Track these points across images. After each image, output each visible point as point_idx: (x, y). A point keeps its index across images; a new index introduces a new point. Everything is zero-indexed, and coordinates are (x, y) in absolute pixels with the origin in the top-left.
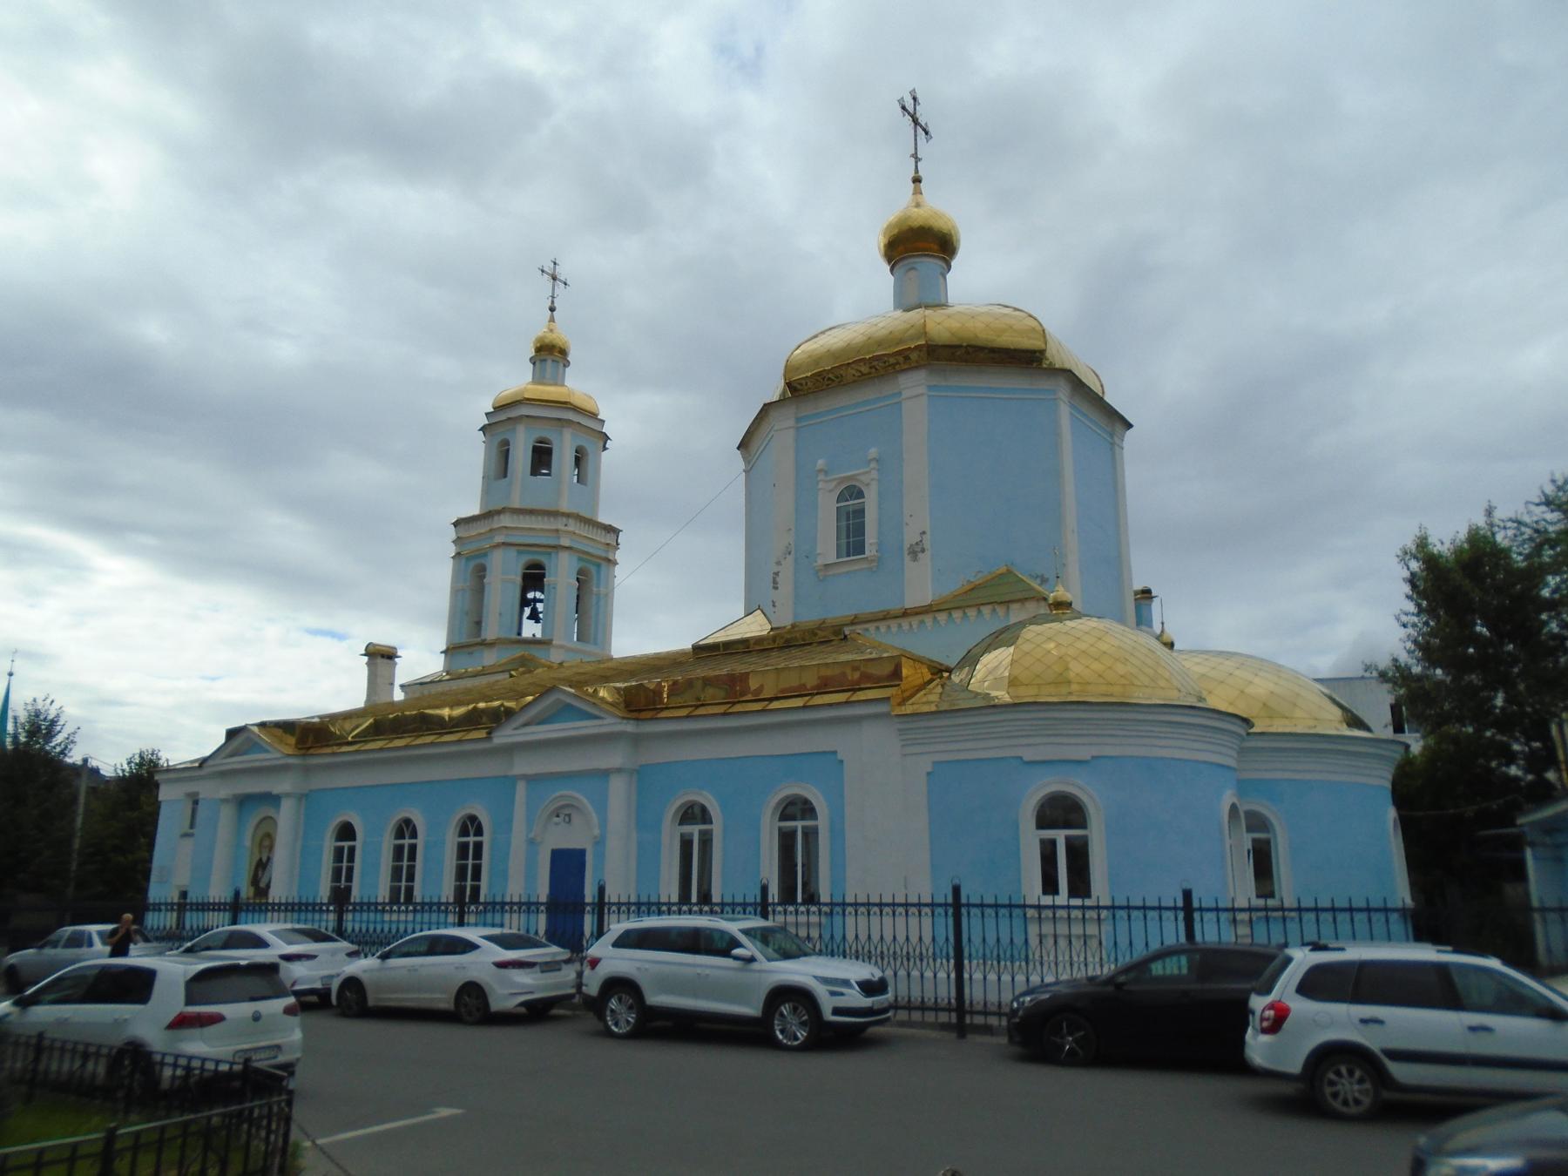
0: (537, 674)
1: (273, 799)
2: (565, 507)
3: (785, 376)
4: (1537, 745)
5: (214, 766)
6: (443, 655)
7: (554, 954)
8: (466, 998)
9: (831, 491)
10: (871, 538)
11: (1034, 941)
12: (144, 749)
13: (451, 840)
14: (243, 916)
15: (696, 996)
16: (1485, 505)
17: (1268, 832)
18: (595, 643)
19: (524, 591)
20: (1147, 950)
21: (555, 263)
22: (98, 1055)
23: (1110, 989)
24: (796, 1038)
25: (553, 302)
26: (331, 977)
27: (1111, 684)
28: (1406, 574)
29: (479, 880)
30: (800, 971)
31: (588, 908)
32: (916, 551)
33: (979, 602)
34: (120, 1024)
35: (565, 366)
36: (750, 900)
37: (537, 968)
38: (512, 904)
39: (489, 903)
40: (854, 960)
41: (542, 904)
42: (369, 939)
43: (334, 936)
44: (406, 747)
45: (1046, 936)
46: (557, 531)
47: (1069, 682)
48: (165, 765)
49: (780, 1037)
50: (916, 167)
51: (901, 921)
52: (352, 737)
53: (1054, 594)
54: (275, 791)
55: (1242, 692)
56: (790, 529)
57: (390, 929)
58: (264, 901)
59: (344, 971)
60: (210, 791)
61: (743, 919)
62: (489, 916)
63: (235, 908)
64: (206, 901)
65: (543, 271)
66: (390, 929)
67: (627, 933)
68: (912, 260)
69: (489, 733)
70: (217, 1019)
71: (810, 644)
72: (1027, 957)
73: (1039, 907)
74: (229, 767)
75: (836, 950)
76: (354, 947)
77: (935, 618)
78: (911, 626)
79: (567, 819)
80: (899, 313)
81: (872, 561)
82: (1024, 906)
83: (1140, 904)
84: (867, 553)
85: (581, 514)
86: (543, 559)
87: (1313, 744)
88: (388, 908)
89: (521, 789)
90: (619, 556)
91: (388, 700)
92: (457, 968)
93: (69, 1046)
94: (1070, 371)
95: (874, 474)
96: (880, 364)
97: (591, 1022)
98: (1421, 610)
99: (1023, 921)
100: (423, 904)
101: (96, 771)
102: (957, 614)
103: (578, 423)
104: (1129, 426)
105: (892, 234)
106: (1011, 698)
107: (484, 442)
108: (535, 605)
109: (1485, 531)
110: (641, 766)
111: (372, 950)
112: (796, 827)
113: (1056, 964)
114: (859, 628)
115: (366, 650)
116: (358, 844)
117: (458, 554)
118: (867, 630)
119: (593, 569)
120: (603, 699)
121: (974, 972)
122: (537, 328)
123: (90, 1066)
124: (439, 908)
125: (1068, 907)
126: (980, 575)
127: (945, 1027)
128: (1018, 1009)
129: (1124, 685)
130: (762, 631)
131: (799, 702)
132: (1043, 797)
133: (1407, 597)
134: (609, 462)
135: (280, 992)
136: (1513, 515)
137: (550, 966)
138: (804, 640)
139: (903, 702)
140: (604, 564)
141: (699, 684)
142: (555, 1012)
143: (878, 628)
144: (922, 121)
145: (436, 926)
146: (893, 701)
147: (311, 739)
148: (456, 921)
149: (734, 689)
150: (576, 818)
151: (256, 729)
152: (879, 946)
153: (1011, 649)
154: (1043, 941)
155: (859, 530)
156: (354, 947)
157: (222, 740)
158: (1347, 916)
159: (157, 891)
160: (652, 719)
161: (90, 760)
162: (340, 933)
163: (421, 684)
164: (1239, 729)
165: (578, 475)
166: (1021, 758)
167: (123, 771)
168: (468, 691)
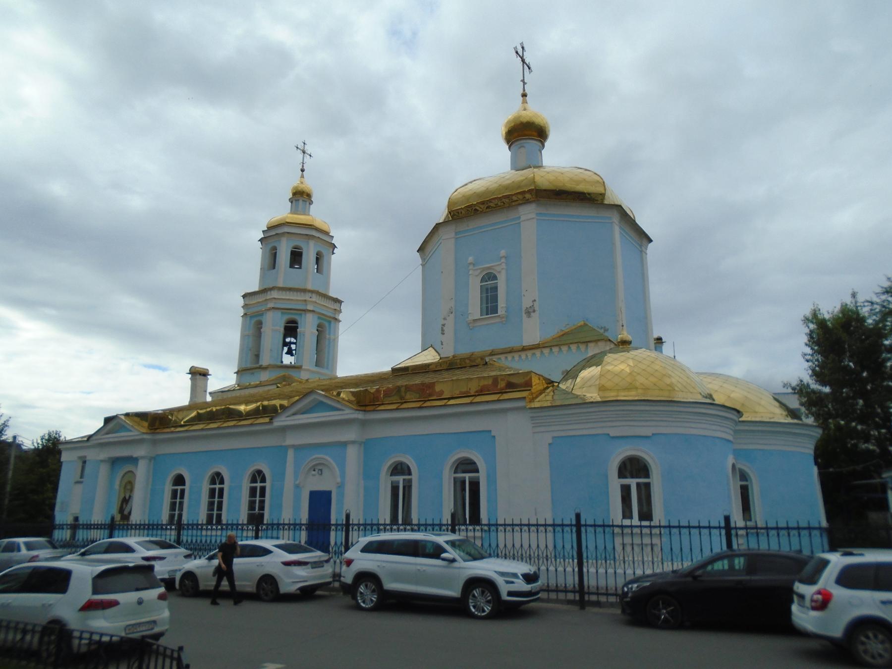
0: (294, 386)
1: (134, 460)
2: (310, 287)
3: (448, 207)
4: (883, 431)
5: (96, 440)
6: (236, 374)
7: (320, 557)
8: (264, 584)
9: (477, 276)
10: (501, 304)
11: (619, 548)
12: (51, 431)
13: (206, 487)
14: (116, 532)
15: (417, 583)
16: (850, 292)
17: (747, 480)
18: (327, 368)
19: (285, 337)
20: (712, 553)
21: (304, 144)
22: (33, 632)
23: (690, 579)
24: (484, 611)
25: (303, 166)
26: (176, 571)
27: (662, 390)
28: (807, 331)
29: (182, 510)
30: (486, 568)
31: (333, 527)
32: (529, 312)
33: (569, 342)
34: (46, 607)
35: (310, 204)
36: (567, 522)
37: (309, 566)
38: (284, 524)
39: (270, 524)
40: (512, 560)
41: (303, 525)
42: (192, 546)
43: (175, 544)
44: (219, 428)
45: (626, 544)
46: (305, 301)
47: (637, 388)
48: (64, 440)
49: (473, 610)
50: (524, 87)
51: (509, 535)
52: (184, 422)
53: (622, 336)
54: (135, 455)
55: (729, 397)
56: (452, 299)
57: (196, 540)
58: (126, 523)
59: (184, 568)
60: (92, 455)
61: (446, 534)
62: (269, 532)
63: (111, 527)
64: (89, 523)
65: (297, 148)
66: (196, 540)
67: (371, 543)
68: (522, 141)
69: (271, 419)
70: (114, 603)
71: (465, 367)
72: (615, 558)
73: (622, 527)
74: (106, 440)
75: (500, 554)
76: (189, 552)
77: (542, 352)
78: (527, 356)
79: (320, 472)
80: (513, 171)
81: (503, 317)
82: (613, 526)
83: (677, 524)
84: (499, 313)
85: (320, 291)
86: (296, 317)
87: (768, 428)
88: (205, 527)
89: (291, 454)
90: (341, 317)
91: (204, 401)
92: (258, 566)
93: (12, 625)
94: (620, 206)
95: (504, 266)
96: (507, 201)
97: (348, 600)
98: (815, 352)
99: (612, 535)
100: (227, 525)
101: (19, 446)
102: (555, 349)
103: (319, 237)
104: (650, 241)
105: (511, 126)
106: (600, 398)
107: (261, 248)
108: (290, 346)
109: (851, 306)
110: (366, 439)
111: (199, 554)
112: (465, 478)
113: (634, 562)
114: (495, 358)
115: (190, 371)
116: (187, 488)
117: (245, 314)
118: (500, 359)
119: (327, 324)
120: (343, 399)
121: (590, 569)
122: (294, 181)
123: (28, 637)
124: (197, 527)
125: (641, 526)
126: (568, 326)
127: (569, 602)
128: (627, 593)
129: (670, 390)
130: (435, 359)
131: (467, 400)
132: (625, 457)
133: (806, 345)
134: (337, 261)
135: (153, 585)
136: (869, 299)
137: (317, 564)
138: (460, 364)
139: (532, 400)
140: (333, 322)
141: (403, 389)
142: (318, 593)
143: (506, 358)
144: (527, 61)
145: (245, 539)
146: (527, 400)
147: (157, 423)
148: (254, 535)
149: (426, 394)
150: (326, 472)
151: (123, 417)
152: (528, 551)
153: (599, 368)
154: (625, 548)
155: (495, 299)
156: (189, 552)
157: (102, 424)
158: (667, 530)
159: (62, 516)
160: (374, 410)
161: (17, 437)
162: (179, 542)
163: (222, 392)
164: (733, 416)
165: (317, 269)
166: (608, 434)
167: (38, 444)
168: (253, 396)
